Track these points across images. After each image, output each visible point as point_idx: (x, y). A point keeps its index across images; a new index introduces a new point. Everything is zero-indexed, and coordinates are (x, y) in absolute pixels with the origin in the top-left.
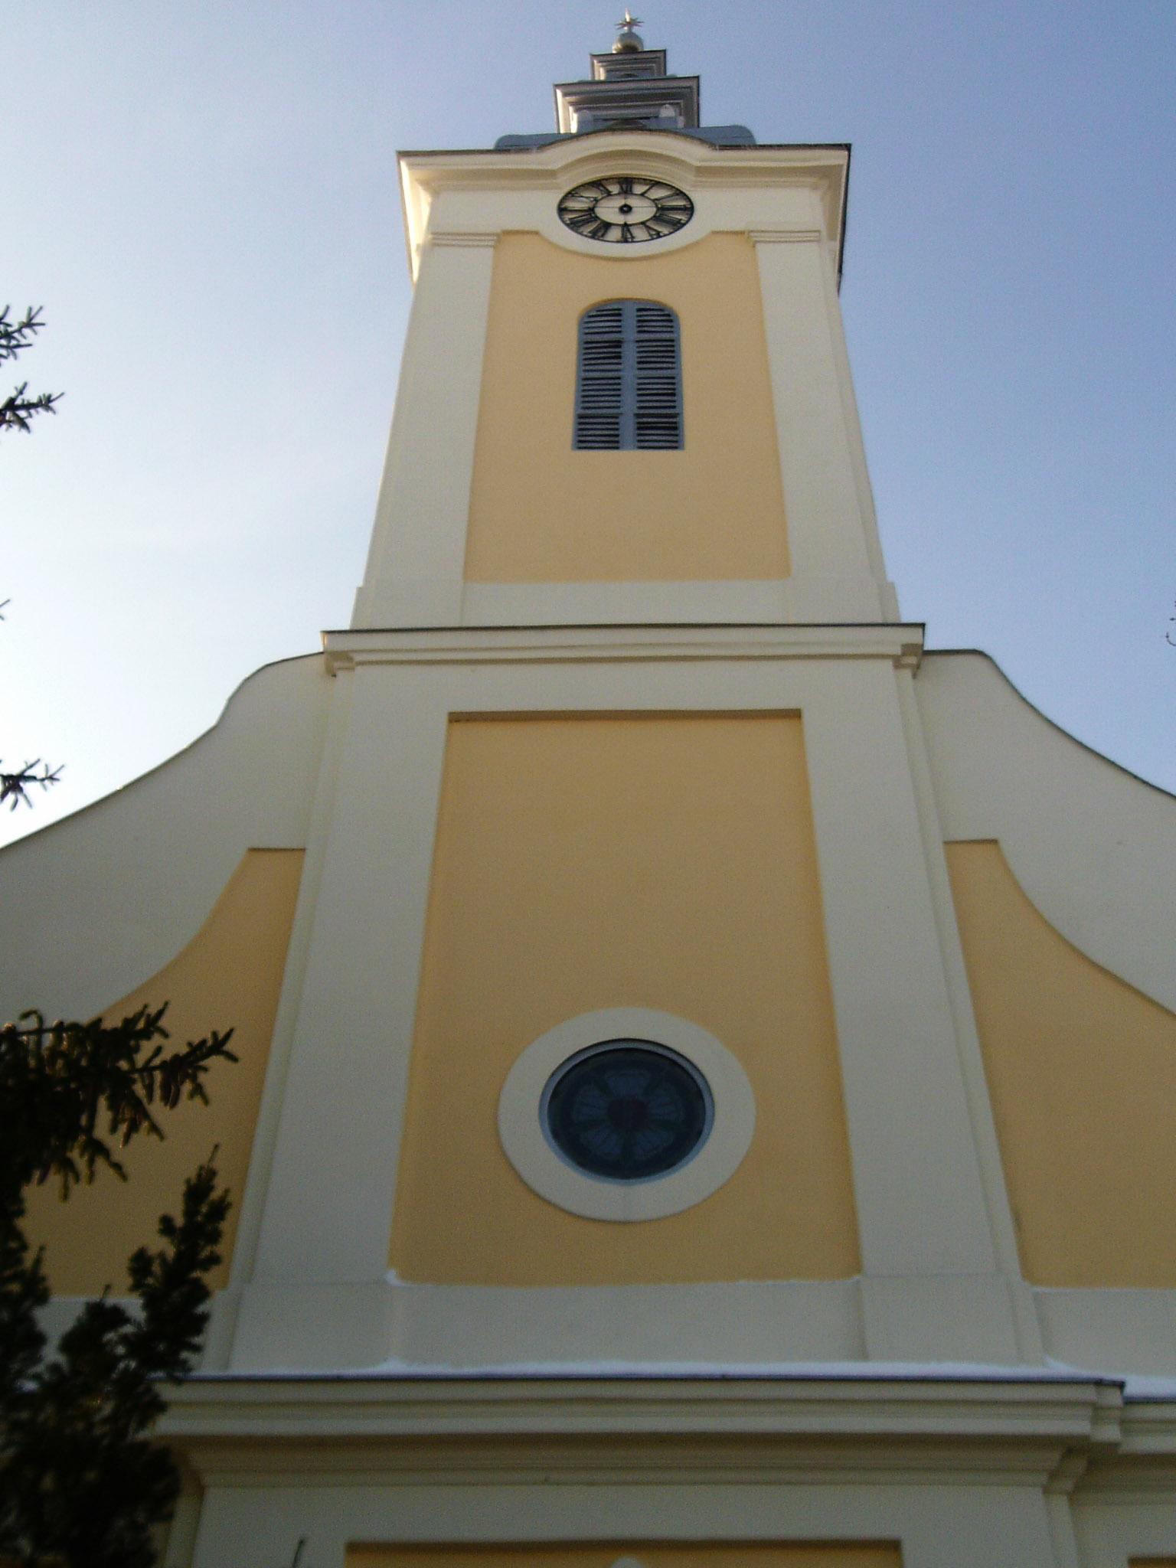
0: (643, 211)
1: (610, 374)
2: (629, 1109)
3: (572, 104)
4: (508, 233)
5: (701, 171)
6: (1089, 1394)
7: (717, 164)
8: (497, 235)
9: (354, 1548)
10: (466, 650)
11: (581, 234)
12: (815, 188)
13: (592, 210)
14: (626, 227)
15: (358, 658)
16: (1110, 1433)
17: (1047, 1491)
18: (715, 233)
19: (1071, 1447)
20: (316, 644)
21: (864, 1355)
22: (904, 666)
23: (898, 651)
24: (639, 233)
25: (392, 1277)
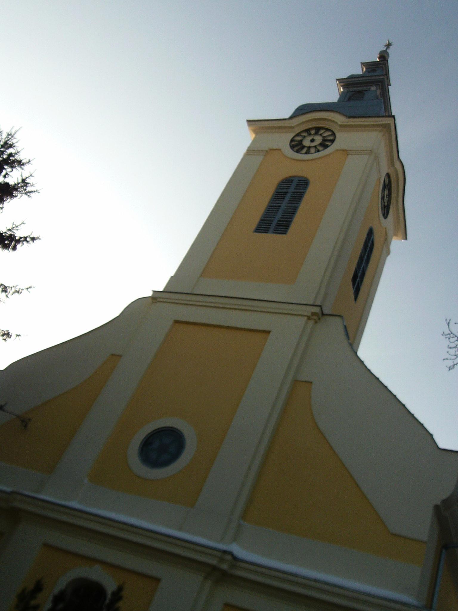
0: (318, 139)
1: (277, 205)
2: (162, 447)
3: (342, 86)
4: (271, 150)
5: (341, 126)
6: (219, 554)
7: (348, 124)
8: (267, 151)
9: (226, 605)
10: (184, 300)
11: (293, 150)
12: (380, 131)
13: (301, 141)
14: (315, 147)
15: (159, 300)
16: (224, 566)
17: (206, 578)
18: (337, 150)
19: (214, 568)
20: (150, 294)
21: (180, 529)
22: (311, 319)
23: (309, 314)
24: (320, 148)
25: (86, 480)
